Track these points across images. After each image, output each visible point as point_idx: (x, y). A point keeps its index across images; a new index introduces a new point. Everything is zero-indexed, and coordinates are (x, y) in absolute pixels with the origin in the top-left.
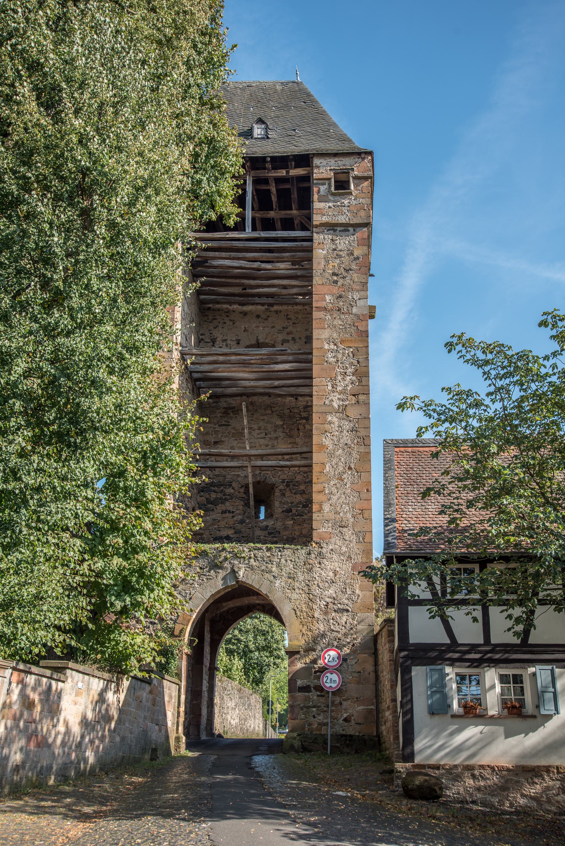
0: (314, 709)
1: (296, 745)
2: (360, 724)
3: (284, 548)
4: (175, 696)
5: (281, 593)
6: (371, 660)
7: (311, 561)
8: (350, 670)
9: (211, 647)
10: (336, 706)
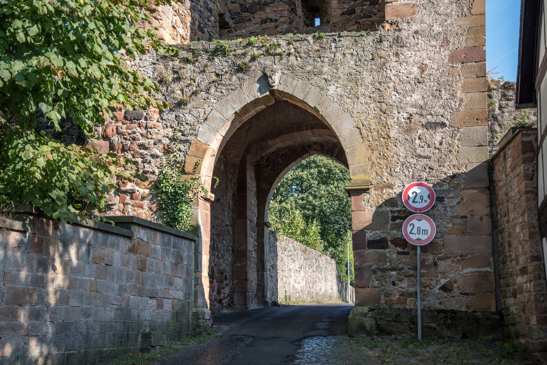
0: (394, 273)
1: (367, 325)
2: (467, 294)
3: (340, 36)
4: (189, 256)
5: (336, 105)
6: (484, 198)
7: (383, 53)
8: (449, 214)
9: (257, 198)
10: (428, 267)
